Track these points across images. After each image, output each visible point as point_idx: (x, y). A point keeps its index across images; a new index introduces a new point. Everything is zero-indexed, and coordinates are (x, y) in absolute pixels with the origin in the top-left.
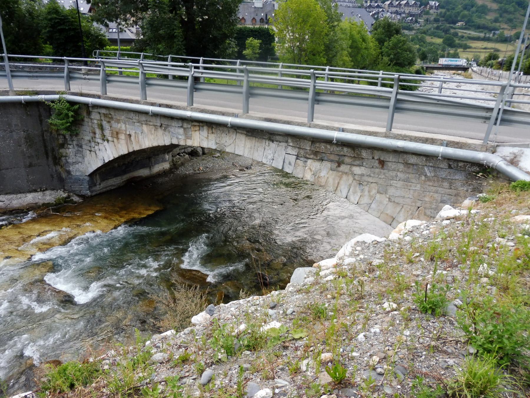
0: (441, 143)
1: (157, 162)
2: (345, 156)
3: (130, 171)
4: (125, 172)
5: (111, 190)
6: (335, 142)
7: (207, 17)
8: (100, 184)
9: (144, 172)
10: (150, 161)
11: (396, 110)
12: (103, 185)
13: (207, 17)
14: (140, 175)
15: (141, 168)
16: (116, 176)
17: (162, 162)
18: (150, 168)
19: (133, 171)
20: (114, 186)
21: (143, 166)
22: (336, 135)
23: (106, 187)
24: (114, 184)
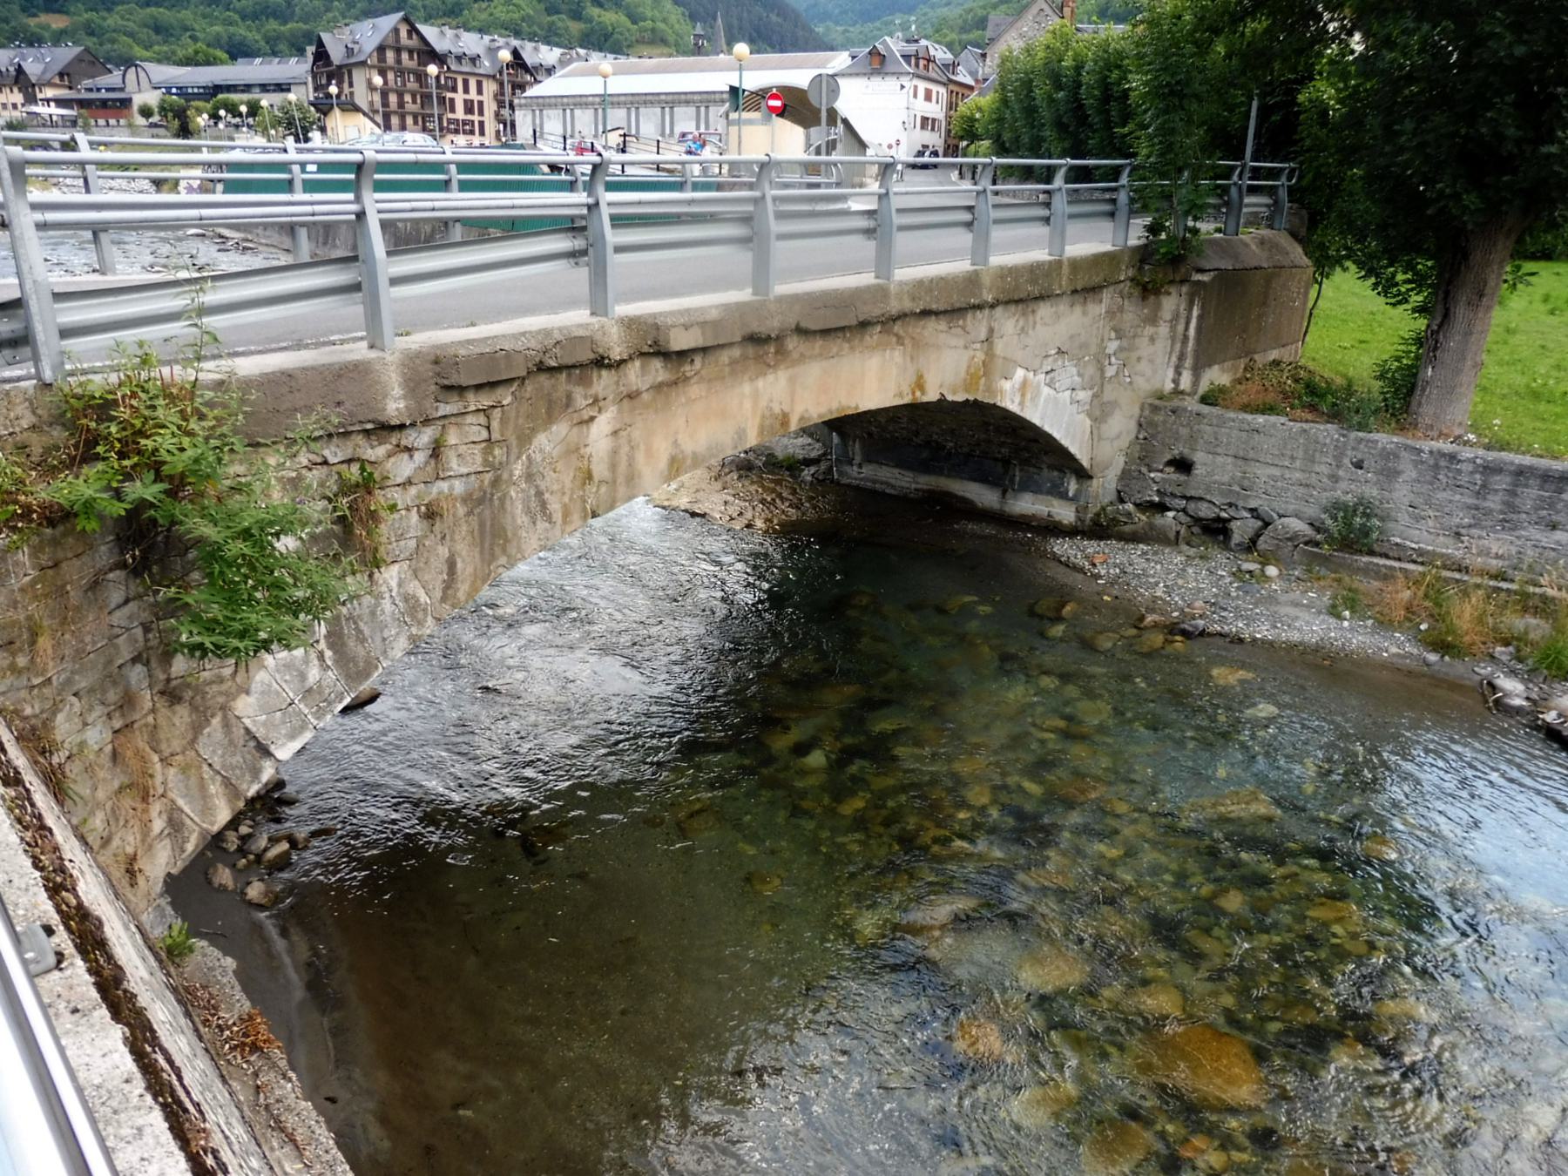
0: (1187, 329)
1: (1029, 486)
2: (1201, 499)
3: (939, 472)
4: (925, 468)
5: (884, 494)
6: (792, 343)
7: (1429, 212)
8: (860, 466)
9: (983, 496)
10: (1006, 472)
11: (21, 334)
12: (868, 471)
13: (1429, 212)
14: (968, 495)
15: (975, 480)
16: (902, 464)
17: (1050, 493)
18: (1004, 493)
19: (948, 476)
20: (893, 487)
21: (983, 478)
22: (51, 233)
23: (874, 482)
24: (893, 481)
